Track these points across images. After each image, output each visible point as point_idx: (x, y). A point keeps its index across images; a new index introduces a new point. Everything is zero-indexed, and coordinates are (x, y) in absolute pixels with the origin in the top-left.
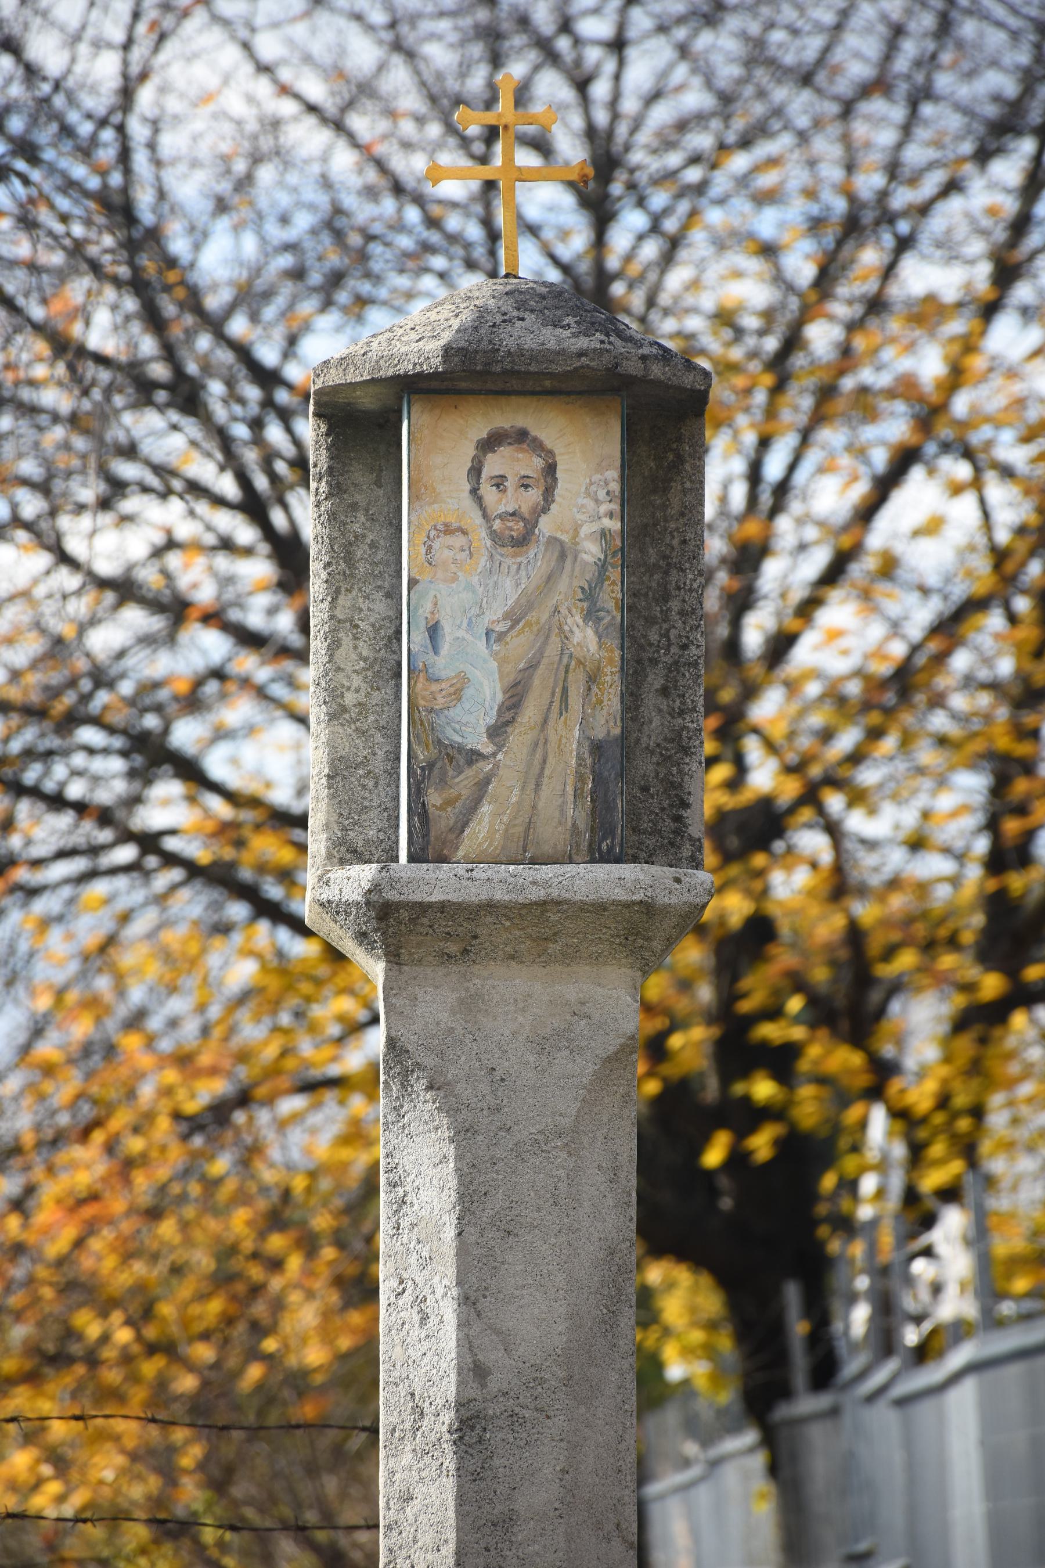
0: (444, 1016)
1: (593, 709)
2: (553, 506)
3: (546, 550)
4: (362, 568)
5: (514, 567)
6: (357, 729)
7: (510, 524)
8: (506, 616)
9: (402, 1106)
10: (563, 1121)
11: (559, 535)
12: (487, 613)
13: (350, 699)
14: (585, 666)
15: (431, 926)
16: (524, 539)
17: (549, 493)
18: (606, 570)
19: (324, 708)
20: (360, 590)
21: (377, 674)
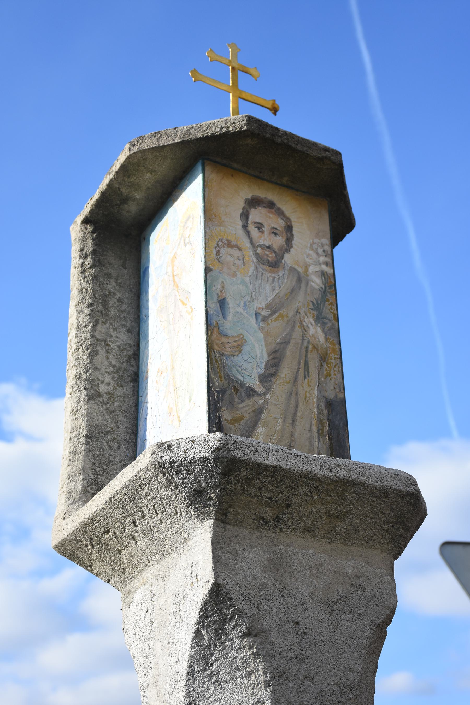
0: (258, 572)
1: (325, 378)
2: (292, 250)
3: (289, 274)
4: (113, 312)
5: (271, 279)
6: (107, 409)
7: (267, 253)
8: (268, 307)
9: (211, 655)
10: (353, 676)
11: (296, 267)
12: (255, 302)
13: (103, 388)
14: (318, 350)
15: (260, 489)
16: (276, 264)
17: (289, 240)
18: (326, 295)
19: (84, 392)
20: (111, 324)
21: (121, 377)
